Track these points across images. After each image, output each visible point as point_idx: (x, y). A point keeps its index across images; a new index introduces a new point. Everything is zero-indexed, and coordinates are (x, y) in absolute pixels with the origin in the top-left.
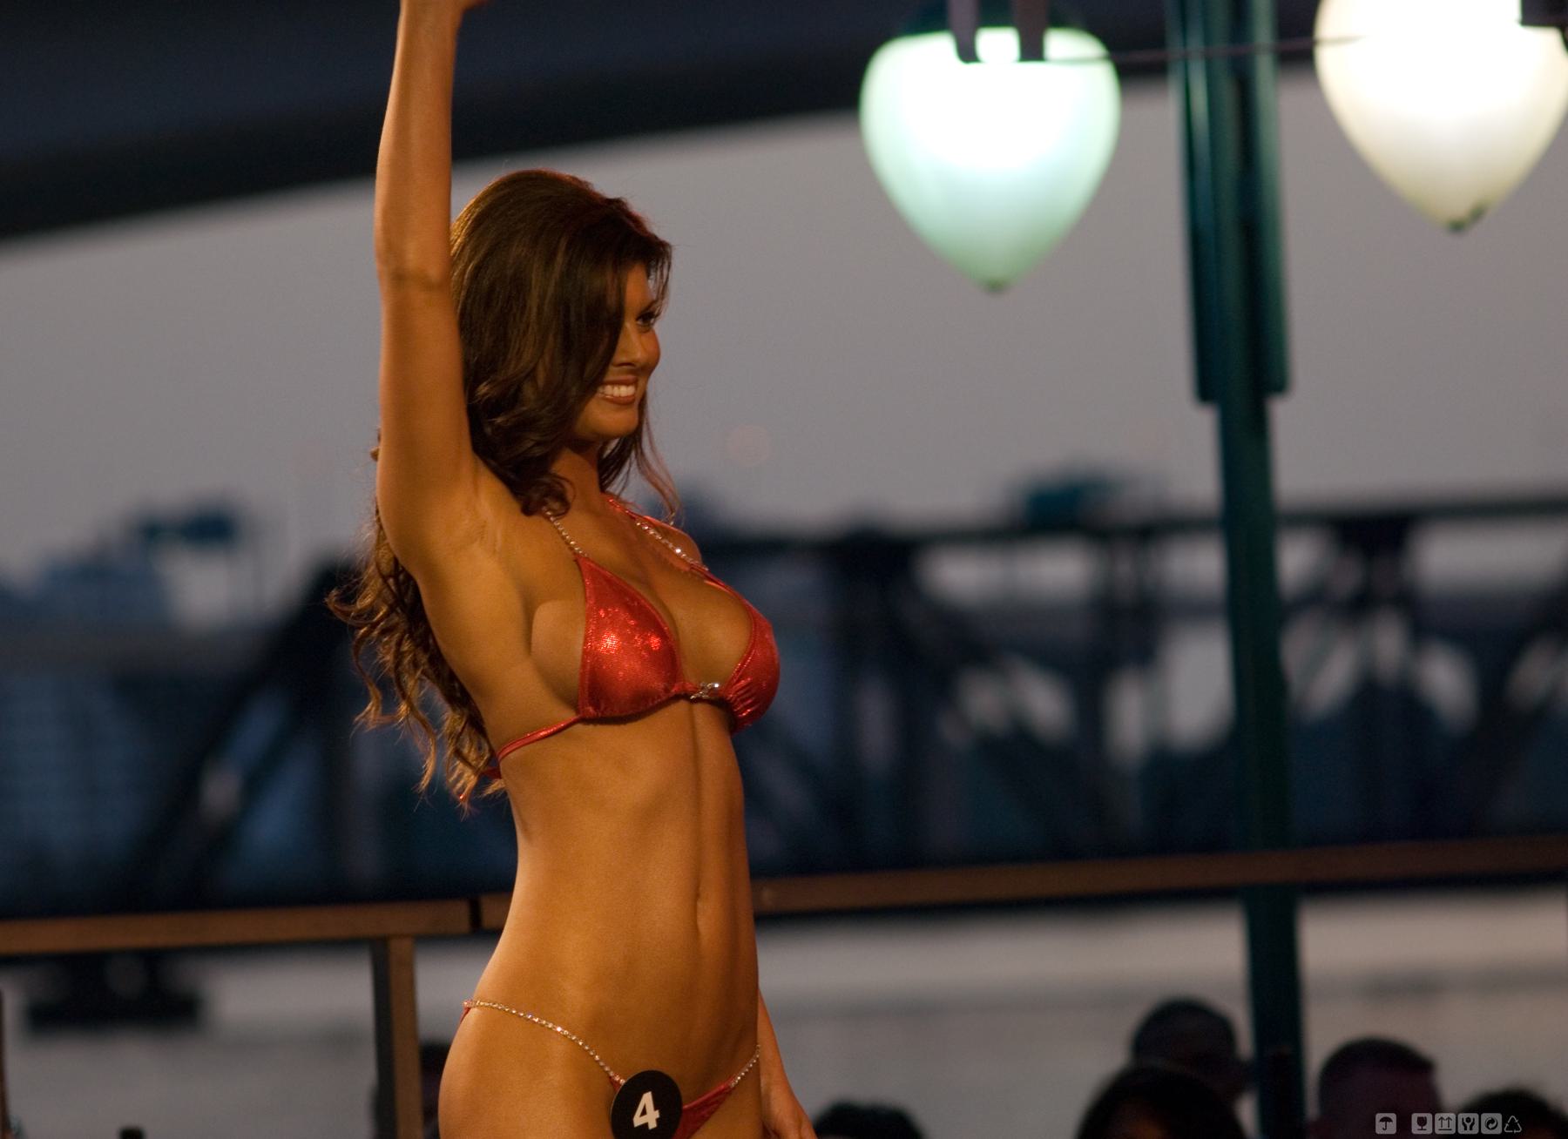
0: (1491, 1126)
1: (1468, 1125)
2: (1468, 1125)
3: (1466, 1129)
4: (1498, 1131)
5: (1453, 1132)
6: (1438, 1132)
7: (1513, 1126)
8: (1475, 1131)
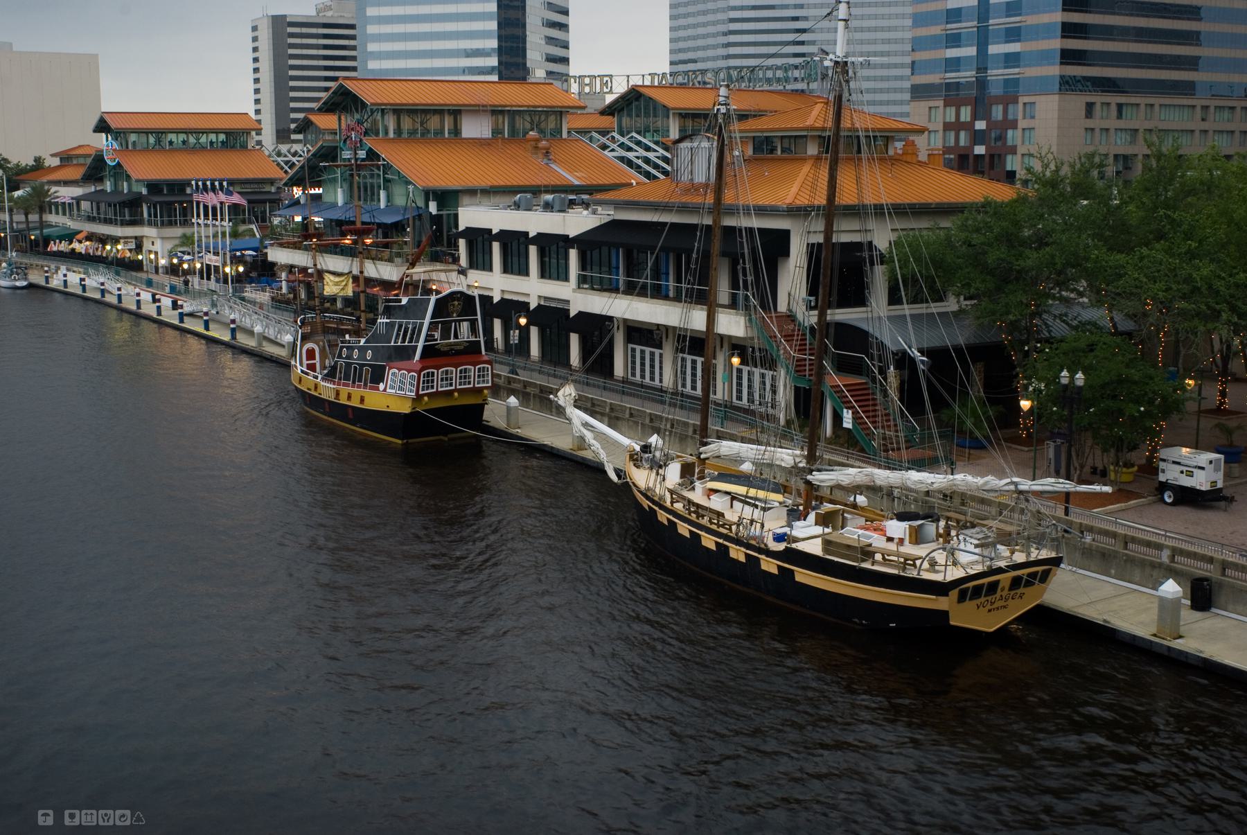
0: (122, 819)
1: (106, 818)
2: (106, 818)
3: (104, 821)
4: (128, 823)
5: (95, 824)
6: (83, 824)
7: (139, 819)
8: (111, 823)
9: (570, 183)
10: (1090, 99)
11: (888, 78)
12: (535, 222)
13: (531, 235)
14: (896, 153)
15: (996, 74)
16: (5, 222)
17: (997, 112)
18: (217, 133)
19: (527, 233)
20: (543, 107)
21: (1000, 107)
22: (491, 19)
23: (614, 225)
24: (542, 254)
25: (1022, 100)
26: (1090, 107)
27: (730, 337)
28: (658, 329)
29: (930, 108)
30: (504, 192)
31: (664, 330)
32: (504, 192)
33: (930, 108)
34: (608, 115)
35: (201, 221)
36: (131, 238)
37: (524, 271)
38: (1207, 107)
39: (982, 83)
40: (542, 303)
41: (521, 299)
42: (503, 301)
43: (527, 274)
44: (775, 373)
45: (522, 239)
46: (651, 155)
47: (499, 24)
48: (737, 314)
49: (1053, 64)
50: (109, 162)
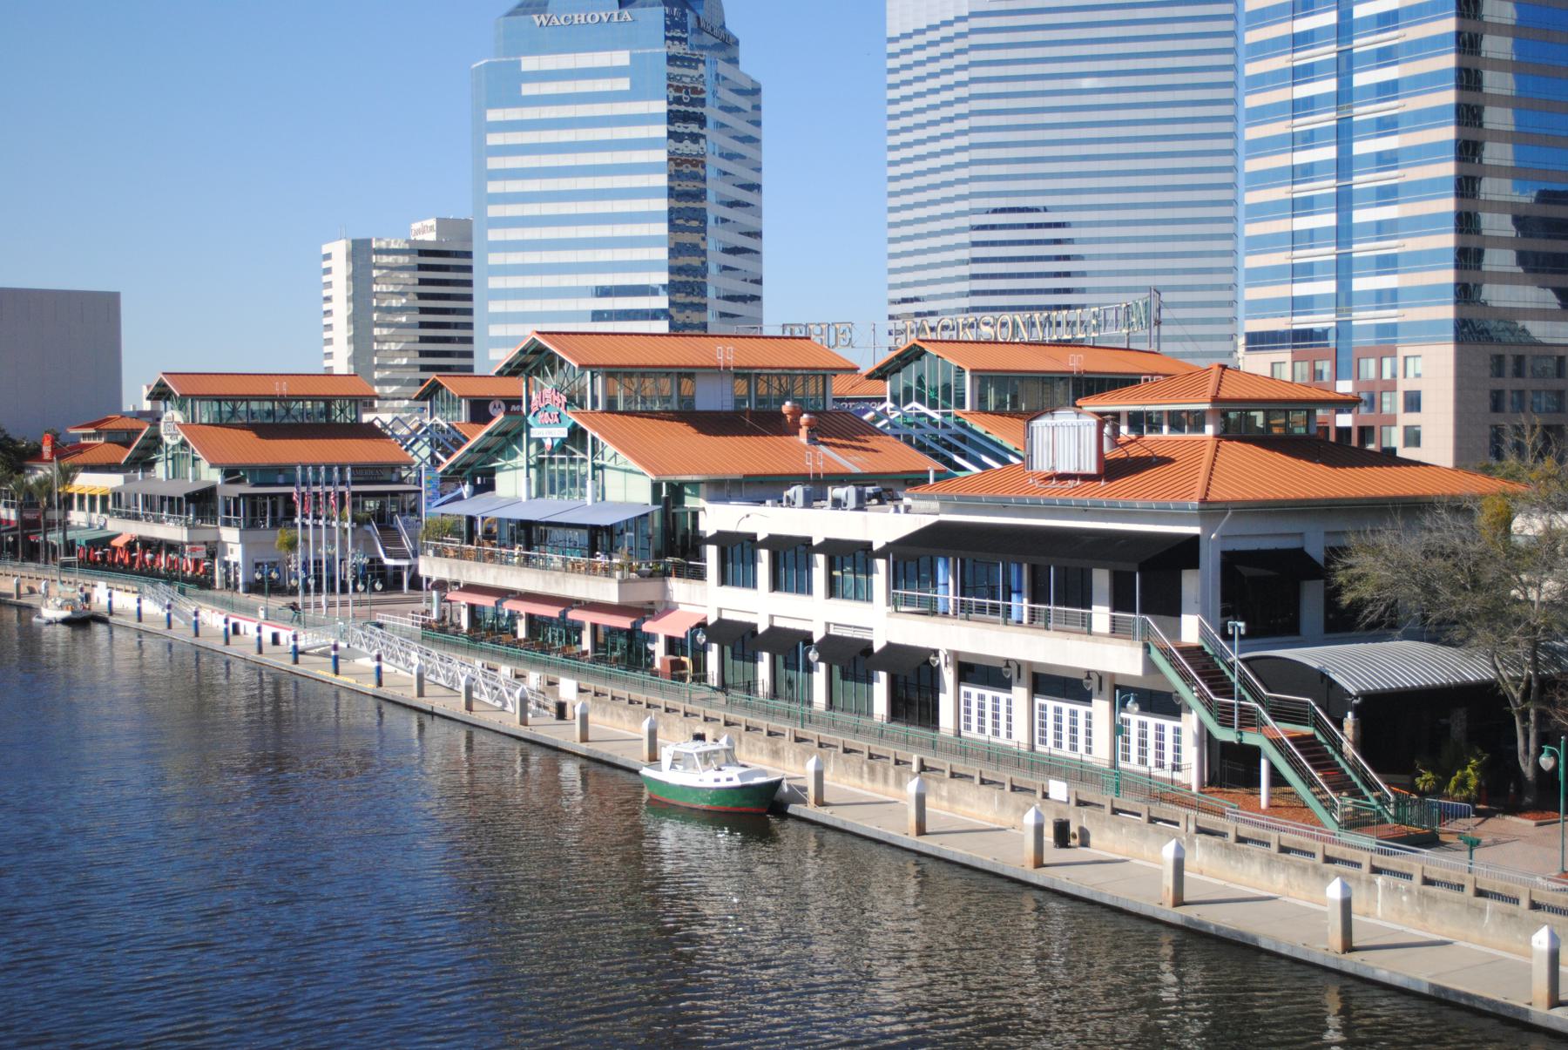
9: (843, 471)
11: (1192, 322)
12: (765, 520)
13: (759, 538)
14: (769, 394)
15: (1364, 318)
16: (355, 545)
17: (1369, 368)
18: (219, 401)
19: (810, 539)
20: (802, 369)
21: (1372, 363)
22: (660, 245)
23: (939, 527)
24: (831, 566)
25: (1402, 351)
27: (1113, 676)
28: (1089, 677)
29: (1273, 364)
30: (761, 482)
31: (1095, 679)
32: (761, 482)
33: (1273, 364)
34: (878, 378)
35: (308, 522)
36: (200, 543)
37: (805, 588)
39: (1343, 330)
40: (832, 632)
41: (858, 635)
42: (772, 630)
43: (869, 599)
44: (689, 679)
45: (801, 548)
47: (671, 251)
48: (1132, 645)
49: (1444, 303)
50: (167, 439)
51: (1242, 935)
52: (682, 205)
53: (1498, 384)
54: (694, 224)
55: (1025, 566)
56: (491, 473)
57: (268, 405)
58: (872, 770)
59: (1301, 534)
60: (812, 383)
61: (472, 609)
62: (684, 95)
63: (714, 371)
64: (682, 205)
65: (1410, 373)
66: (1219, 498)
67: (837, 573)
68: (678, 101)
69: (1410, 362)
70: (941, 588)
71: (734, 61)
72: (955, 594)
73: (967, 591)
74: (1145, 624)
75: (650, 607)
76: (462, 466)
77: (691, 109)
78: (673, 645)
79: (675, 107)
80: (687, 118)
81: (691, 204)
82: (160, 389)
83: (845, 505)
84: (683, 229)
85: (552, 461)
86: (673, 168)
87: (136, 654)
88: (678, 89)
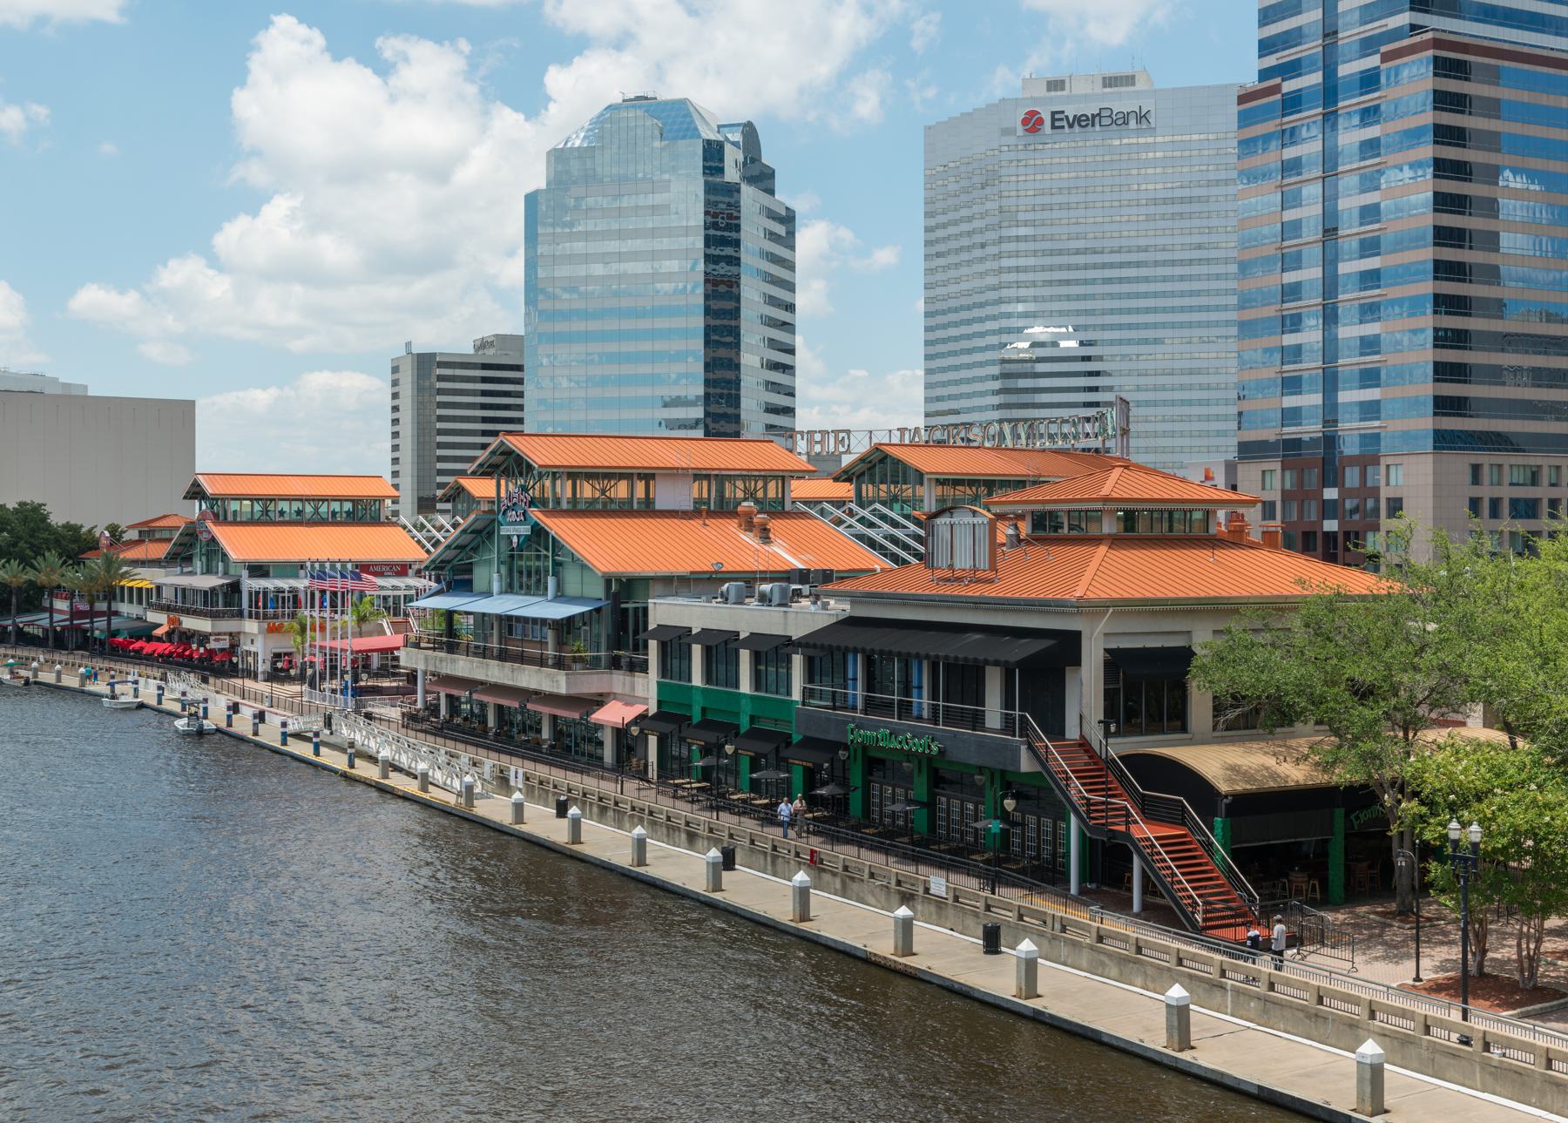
10: (1474, 460)
17: (1352, 477)
18: (251, 500)
21: (1356, 470)
26: (1476, 470)
29: (1264, 472)
33: (1264, 472)
36: (225, 634)
38: (1500, 466)
46: (898, 533)
51: (1222, 1074)
52: (718, 322)
53: (1476, 492)
54: (729, 339)
55: (859, 657)
56: (469, 569)
57: (296, 506)
58: (668, 835)
59: (1189, 632)
60: (772, 485)
61: (500, 709)
62: (720, 220)
63: (673, 473)
64: (718, 322)
65: (1393, 481)
66: (730, 569)
67: (762, 668)
68: (715, 226)
69: (1393, 470)
70: (915, 692)
71: (771, 192)
72: (934, 695)
73: (817, 678)
74: (1022, 718)
75: (599, 699)
76: (442, 562)
77: (726, 234)
78: (620, 733)
79: (712, 232)
80: (724, 242)
81: (725, 322)
82: (194, 489)
83: (770, 601)
84: (719, 344)
85: (521, 557)
86: (710, 287)
87: (1395, 1042)
88: (715, 215)
